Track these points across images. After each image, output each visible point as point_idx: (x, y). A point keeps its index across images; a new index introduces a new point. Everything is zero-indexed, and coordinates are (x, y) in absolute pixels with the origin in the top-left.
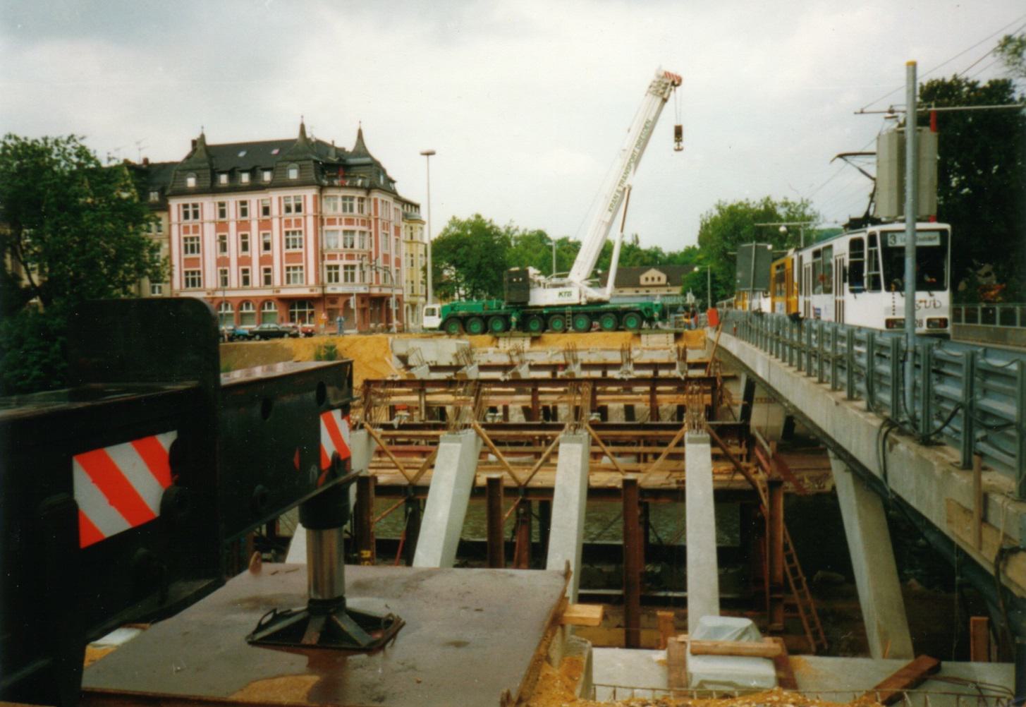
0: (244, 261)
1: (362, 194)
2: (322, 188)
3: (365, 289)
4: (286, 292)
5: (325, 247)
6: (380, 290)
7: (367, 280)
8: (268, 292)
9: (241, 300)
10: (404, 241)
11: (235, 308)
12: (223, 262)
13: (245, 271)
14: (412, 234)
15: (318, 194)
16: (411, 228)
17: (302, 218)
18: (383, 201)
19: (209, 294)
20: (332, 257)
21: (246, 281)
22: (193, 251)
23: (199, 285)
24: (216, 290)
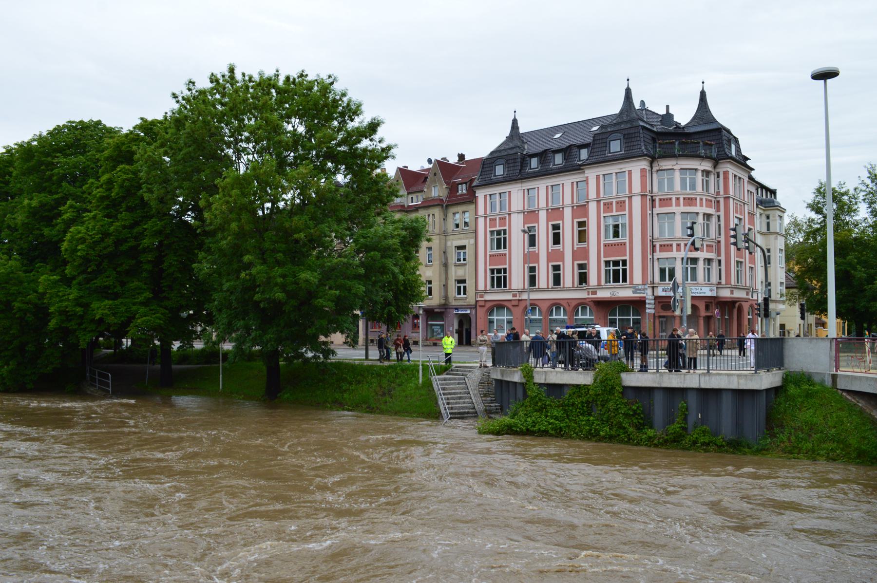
0: (555, 256)
1: (707, 165)
2: (653, 159)
3: (711, 290)
4: (603, 294)
5: (656, 235)
6: (732, 293)
7: (714, 279)
8: (582, 295)
9: (552, 302)
10: (758, 232)
11: (544, 313)
12: (531, 258)
13: (581, 267)
14: (768, 224)
15: (648, 168)
16: (768, 217)
17: (627, 199)
18: (735, 176)
19: (514, 295)
20: (666, 247)
21: (557, 280)
22: (499, 247)
23: (505, 286)
24: (523, 291)
